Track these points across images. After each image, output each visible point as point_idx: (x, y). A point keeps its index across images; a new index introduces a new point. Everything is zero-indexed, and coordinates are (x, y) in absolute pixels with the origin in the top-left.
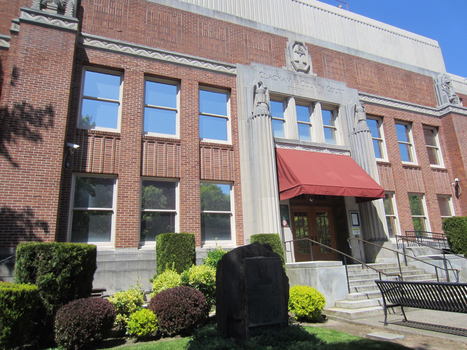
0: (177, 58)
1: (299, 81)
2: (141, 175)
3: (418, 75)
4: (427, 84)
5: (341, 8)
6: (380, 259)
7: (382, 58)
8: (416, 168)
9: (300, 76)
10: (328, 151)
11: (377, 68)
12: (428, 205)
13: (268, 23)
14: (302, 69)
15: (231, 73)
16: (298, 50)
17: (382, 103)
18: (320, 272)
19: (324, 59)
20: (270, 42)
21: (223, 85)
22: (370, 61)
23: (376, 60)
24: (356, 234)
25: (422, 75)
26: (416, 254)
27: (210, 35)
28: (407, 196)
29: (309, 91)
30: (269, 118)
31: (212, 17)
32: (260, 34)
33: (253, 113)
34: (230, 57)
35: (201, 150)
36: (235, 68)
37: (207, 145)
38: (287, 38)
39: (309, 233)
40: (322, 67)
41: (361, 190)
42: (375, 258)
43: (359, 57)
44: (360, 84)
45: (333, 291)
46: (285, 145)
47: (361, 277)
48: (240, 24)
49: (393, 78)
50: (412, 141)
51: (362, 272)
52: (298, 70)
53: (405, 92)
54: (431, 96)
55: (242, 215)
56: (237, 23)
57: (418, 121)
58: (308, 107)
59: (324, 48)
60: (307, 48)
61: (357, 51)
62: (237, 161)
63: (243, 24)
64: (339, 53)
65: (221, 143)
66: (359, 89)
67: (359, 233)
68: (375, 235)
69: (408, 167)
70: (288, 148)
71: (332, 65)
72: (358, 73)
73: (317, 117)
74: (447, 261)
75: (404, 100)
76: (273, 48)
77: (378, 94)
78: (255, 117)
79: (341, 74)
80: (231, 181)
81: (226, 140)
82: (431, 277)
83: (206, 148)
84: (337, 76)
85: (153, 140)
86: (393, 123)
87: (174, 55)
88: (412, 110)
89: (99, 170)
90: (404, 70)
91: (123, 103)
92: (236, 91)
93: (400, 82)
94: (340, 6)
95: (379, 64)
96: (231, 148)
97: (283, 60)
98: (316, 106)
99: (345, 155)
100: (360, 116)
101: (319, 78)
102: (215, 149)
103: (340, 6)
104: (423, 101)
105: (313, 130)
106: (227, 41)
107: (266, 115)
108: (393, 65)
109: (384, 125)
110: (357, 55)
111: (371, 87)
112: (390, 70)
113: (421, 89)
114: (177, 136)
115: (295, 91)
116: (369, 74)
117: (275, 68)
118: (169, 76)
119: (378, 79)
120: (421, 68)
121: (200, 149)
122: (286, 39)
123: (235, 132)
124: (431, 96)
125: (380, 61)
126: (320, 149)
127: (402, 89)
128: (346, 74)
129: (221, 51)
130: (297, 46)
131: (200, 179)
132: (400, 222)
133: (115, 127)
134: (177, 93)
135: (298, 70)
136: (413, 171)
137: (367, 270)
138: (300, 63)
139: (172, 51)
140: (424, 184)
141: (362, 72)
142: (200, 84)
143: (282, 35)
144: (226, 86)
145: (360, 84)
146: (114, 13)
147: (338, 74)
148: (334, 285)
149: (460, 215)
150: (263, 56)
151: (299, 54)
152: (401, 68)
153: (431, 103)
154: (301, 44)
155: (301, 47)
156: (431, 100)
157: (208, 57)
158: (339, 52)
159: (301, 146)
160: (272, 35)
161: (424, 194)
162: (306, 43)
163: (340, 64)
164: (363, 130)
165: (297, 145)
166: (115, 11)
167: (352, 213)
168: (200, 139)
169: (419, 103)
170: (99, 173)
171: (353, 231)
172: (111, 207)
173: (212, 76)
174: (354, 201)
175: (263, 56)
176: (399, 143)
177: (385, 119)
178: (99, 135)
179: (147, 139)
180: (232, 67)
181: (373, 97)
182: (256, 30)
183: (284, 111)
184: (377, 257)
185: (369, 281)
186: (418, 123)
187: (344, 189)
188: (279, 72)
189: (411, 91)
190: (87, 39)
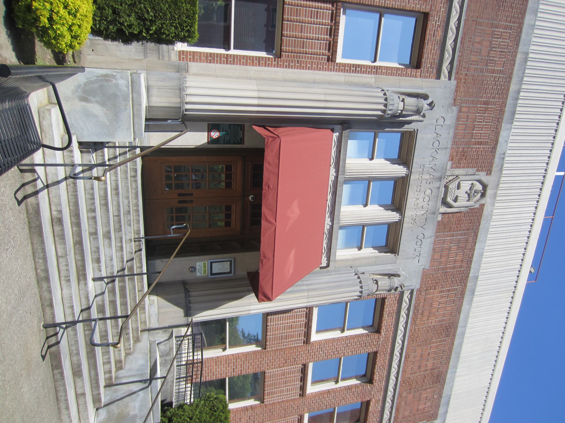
0: (404, 326)
1: (431, 186)
3: (440, 396)
4: (427, 410)
5: (530, 272)
6: (156, 301)
7: (463, 333)
8: (303, 388)
9: (439, 188)
10: (328, 227)
11: (449, 326)
12: (246, 409)
13: (510, 145)
14: (449, 194)
15: (443, 70)
16: (475, 188)
17: (399, 332)
18: (122, 78)
19: (462, 229)
21: (425, 55)
22: (459, 313)
23: (461, 323)
24: (198, 268)
25: (440, 401)
26: (162, 347)
27: (496, 41)
28: (258, 370)
29: (418, 201)
30: (358, 296)
31: (519, 50)
32: (497, 128)
33: (363, 273)
34: (464, 73)
36: (450, 79)
38: (490, 174)
40: (450, 231)
42: (157, 295)
43: (464, 294)
44: (426, 294)
45: (84, 104)
46: (337, 148)
47: (116, 214)
48: (510, 94)
49: (435, 353)
50: (342, 384)
51: (129, 228)
52: (446, 187)
53: (415, 373)
54: (410, 416)
55: (227, 63)
56: (511, 89)
57: (374, 392)
58: (386, 245)
59: (477, 236)
60: (477, 206)
61: (473, 292)
62: (312, 65)
63: (509, 101)
65: (340, 35)
66: (419, 291)
67: (198, 274)
68: (195, 296)
69: (304, 375)
70: (333, 154)
71: (454, 248)
72: (441, 292)
73: (377, 213)
74: (146, 385)
75: (404, 371)
76: (478, 150)
77: (412, 324)
78: (359, 278)
79: (440, 263)
80: (281, 51)
81: (318, 331)
82: (118, 358)
83: (332, 14)
84: (437, 256)
85: (334, 36)
86: (371, 350)
88: (390, 384)
90: (447, 372)
91: (377, 67)
92: (416, 77)
93: (430, 364)
94: (533, 271)
95: (456, 328)
96: (331, 58)
97: (460, 163)
98: (395, 213)
99: (323, 256)
100: (383, 282)
101: (436, 223)
102: (331, 29)
103: (533, 271)
104: (403, 403)
105: (359, 208)
106: (488, 71)
107: (361, 292)
108: (453, 354)
109: (367, 335)
110: (467, 293)
111: (422, 314)
112: (447, 348)
113: (419, 401)
115: (417, 177)
116: (441, 312)
117: (449, 146)
119: (434, 326)
120: (449, 401)
122: (489, 172)
123: (356, 69)
124: (410, 416)
125: (459, 330)
126: (331, 213)
127: (420, 367)
128: (440, 272)
129: (473, 58)
130: (479, 187)
132: (218, 357)
133: (343, 57)
135: (446, 187)
136: (298, 384)
137: (131, 240)
138: (457, 191)
140: (279, 403)
143: (494, 165)
144: (423, 60)
145: (426, 294)
146: (495, 38)
147: (441, 257)
148: (96, 108)
150: (465, 130)
151: (470, 189)
152: (450, 367)
153: (400, 416)
154: (483, 195)
155: (480, 194)
156: (405, 418)
157: (464, 34)
158: (471, 262)
159: (337, 177)
160: (495, 148)
161: (263, 402)
162: (484, 205)
163: (455, 261)
164: (363, 284)
165: (337, 172)
167: (231, 261)
169: (400, 395)
171: (202, 264)
172: (235, 48)
173: (438, 38)
174: (252, 269)
175: (465, 130)
176: (340, 359)
177: (376, 335)
178: (335, 18)
180: (450, 73)
181: (408, 315)
182: (502, 122)
183: (380, 206)
184: (159, 298)
185: (109, 217)
186: (370, 393)
188: (444, 151)
189: (417, 383)
190: (449, 66)
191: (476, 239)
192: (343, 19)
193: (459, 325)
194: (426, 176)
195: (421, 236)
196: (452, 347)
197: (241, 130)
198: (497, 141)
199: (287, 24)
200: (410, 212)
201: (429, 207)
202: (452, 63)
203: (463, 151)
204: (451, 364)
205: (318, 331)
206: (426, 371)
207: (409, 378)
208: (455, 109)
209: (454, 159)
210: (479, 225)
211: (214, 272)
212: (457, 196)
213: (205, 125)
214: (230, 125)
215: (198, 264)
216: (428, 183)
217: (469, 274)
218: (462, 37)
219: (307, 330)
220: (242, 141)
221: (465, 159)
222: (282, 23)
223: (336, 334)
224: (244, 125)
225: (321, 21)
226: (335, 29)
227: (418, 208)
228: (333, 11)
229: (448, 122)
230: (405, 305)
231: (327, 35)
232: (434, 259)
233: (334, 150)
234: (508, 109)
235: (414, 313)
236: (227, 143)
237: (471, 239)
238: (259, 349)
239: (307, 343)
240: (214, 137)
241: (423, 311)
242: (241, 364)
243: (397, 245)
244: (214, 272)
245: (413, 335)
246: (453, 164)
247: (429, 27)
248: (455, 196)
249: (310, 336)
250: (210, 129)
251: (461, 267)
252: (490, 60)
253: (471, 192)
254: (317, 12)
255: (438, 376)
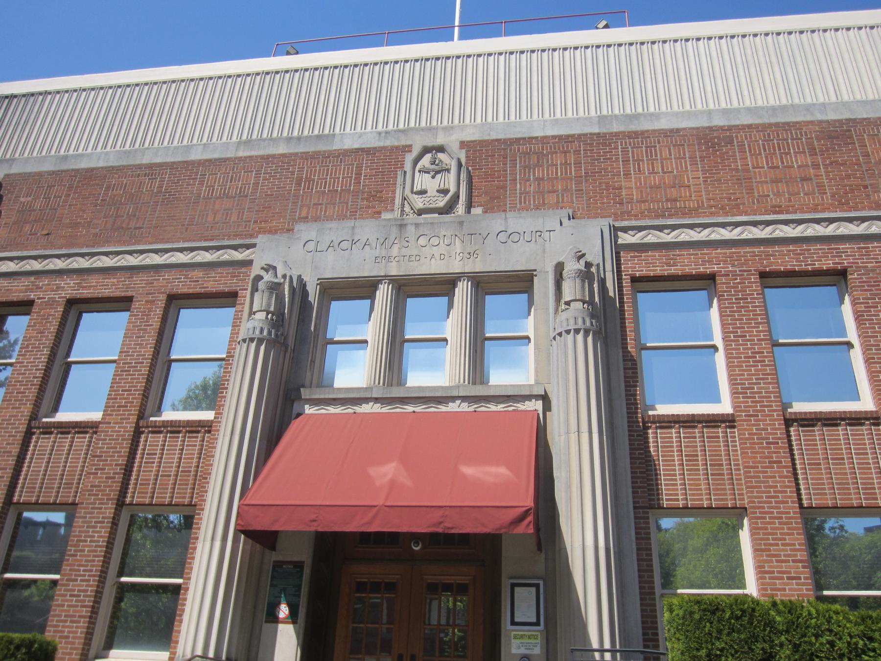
1: (412, 239)
2: (801, 506)
5: (606, 26)
9: (417, 225)
17: (714, 237)
20: (359, 167)
24: (523, 651)
29: (436, 256)
35: (792, 433)
37: (155, 427)
39: (593, 656)
40: (504, 187)
41: (441, 512)
48: (291, 151)
52: (420, 212)
59: (518, 140)
63: (301, 149)
64: (568, 139)
67: (537, 651)
69: (819, 420)
71: (538, 173)
72: (627, 175)
75: (815, 210)
77: (698, 216)
80: (736, 508)
81: (856, 397)
83: (661, 428)
84: (552, 199)
85: (179, 426)
87: (786, 222)
89: (702, 500)
94: (601, 25)
114: (725, 407)
118: (112, 295)
119: (704, 171)
121: (788, 432)
125: (718, 121)
130: (426, 160)
131: (801, 506)
133: (717, 400)
134: (711, 306)
139: (134, 244)
141: (645, 167)
142: (763, 275)
143: (396, 144)
144: (226, 290)
149: (798, 589)
151: (428, 173)
154: (441, 149)
158: (568, 136)
159: (376, 400)
164: (562, 330)
166: (557, 169)
168: (786, 406)
170: (679, 508)
171: (515, 643)
173: (201, 274)
179: (654, 422)
181: (674, 227)
187: (376, 509)
188: (357, 230)
191: (524, 139)
192: (663, 409)
193: (706, 124)
194: (395, 251)
195: (503, 237)
196: (757, 126)
197: (281, 566)
198: (358, 150)
199: (138, 497)
200: (456, 266)
201: (448, 234)
202: (235, 248)
203: (367, 200)
204: (800, 119)
205: (856, 397)
206: (816, 166)
207: (833, 196)
208: (297, 227)
209: (378, 209)
210: (498, 140)
211: (534, 620)
212: (438, 191)
213: (267, 627)
214: (271, 585)
215: (514, 651)
216: (406, 244)
217: (594, 134)
218: (205, 240)
219: (700, 422)
220: (299, 566)
221: (381, 192)
222: (156, 505)
223: (857, 356)
224: (274, 562)
225: (676, 453)
226: (172, 426)
227: (449, 252)
228: (149, 432)
229: (313, 235)
230: (652, 237)
231: (178, 437)
232: (558, 202)
233: (332, 410)
234: (311, 148)
235: (671, 216)
236: (299, 590)
237: (523, 148)
238: (746, 522)
239: (734, 421)
240: (287, 612)
241: (667, 200)
242: (777, 561)
243: (517, 276)
244: (534, 620)
245: (723, 208)
246: (386, 210)
247: (186, 290)
248: (438, 194)
249: (713, 415)
250: (273, 618)
251: (577, 152)
252: (240, 192)
253: (433, 171)
254: (148, 454)
255: (830, 137)
